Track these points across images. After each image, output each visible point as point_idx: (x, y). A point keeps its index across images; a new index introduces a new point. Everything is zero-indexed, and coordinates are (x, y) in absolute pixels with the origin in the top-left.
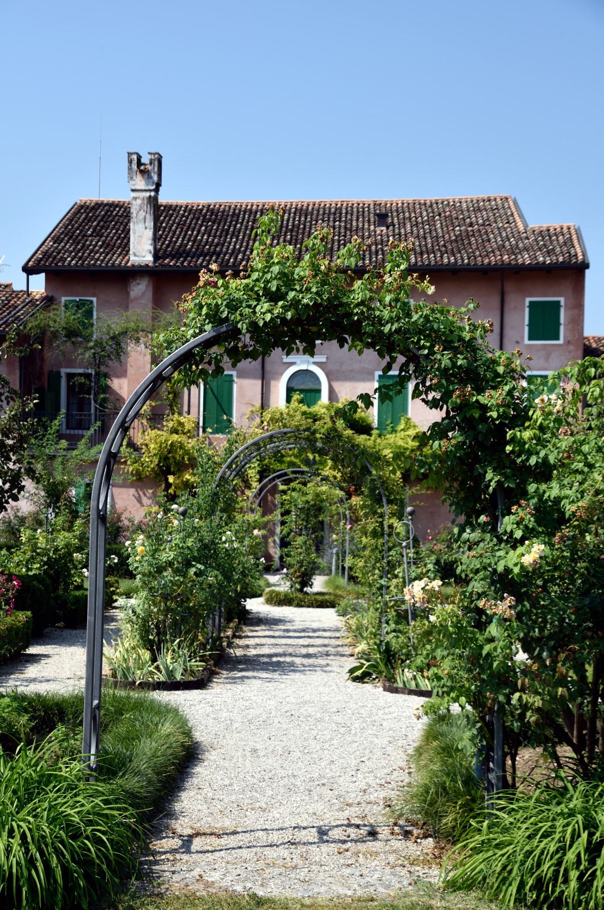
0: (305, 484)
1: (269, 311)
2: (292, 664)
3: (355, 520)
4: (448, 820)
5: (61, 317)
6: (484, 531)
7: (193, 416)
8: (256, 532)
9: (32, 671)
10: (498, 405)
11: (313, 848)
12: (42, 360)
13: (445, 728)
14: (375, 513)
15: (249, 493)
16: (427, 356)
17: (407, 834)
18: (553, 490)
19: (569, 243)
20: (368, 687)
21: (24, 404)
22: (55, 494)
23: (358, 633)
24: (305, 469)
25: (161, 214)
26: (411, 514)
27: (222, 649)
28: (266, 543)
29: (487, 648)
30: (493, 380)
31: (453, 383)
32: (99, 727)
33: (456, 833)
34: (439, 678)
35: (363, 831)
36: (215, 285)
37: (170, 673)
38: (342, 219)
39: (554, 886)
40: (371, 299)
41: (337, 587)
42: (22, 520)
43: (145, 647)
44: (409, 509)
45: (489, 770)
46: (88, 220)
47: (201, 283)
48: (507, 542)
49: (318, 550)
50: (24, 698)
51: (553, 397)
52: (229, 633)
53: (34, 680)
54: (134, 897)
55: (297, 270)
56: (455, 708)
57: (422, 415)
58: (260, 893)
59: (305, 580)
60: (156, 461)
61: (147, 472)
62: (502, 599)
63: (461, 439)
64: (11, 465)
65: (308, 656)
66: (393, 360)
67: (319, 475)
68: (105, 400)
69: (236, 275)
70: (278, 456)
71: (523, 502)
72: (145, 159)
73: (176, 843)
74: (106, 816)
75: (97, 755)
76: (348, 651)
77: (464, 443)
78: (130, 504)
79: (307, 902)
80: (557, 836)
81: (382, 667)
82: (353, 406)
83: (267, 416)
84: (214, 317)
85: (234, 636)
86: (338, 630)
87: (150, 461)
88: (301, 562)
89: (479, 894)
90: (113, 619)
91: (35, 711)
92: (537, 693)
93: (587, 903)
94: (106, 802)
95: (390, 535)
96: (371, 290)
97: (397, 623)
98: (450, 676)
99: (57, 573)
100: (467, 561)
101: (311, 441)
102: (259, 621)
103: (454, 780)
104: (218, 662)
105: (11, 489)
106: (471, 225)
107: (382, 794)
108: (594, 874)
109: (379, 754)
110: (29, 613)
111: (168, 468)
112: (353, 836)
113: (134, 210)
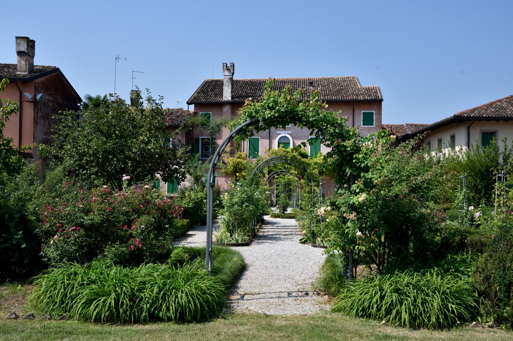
0: (284, 176)
1: (270, 114)
2: (280, 238)
3: (302, 188)
4: (333, 289)
5: (200, 119)
6: (346, 190)
7: (245, 152)
8: (267, 192)
9: (190, 240)
10: (350, 146)
11: (286, 299)
12: (193, 134)
13: (332, 258)
14: (309, 185)
15: (264, 179)
16: (325, 129)
17: (319, 294)
18: (369, 175)
19: (376, 92)
20: (306, 246)
21: (186, 149)
22: (197, 179)
23: (303, 227)
24: (284, 170)
25: (233, 83)
26: (321, 185)
27: (255, 233)
28: (271, 196)
29: (347, 230)
30: (348, 137)
31: (334, 138)
32: (212, 258)
33: (336, 293)
34: (330, 241)
35: (304, 293)
36: (251, 105)
37: (237, 241)
38: (295, 83)
39: (369, 310)
40: (305, 109)
41: (296, 212)
42: (186, 189)
43: (228, 232)
44: (321, 184)
45: (347, 272)
46: (209, 86)
47: (246, 104)
48: (354, 193)
49: (289, 199)
50: (186, 248)
51: (369, 143)
52: (258, 227)
53: (190, 243)
54: (224, 314)
55: (279, 100)
56: (336, 252)
57: (325, 150)
58: (268, 313)
59: (285, 209)
60: (232, 168)
61: (229, 172)
62: (352, 213)
63: (337, 158)
64: (182, 170)
65: (285, 235)
66: (313, 130)
67: (289, 172)
68: (214, 147)
69: (258, 102)
70: (275, 166)
71: (359, 180)
72: (229, 65)
73: (239, 297)
74: (214, 287)
75: (211, 267)
76: (300, 233)
77: (339, 159)
78: (222, 183)
79: (284, 316)
80: (370, 294)
81: (311, 238)
82: (300, 146)
83: (271, 152)
84: (250, 116)
85: (260, 228)
86: (296, 226)
87: (230, 168)
88: (283, 203)
89: (343, 313)
90: (218, 223)
91: (190, 253)
92: (364, 245)
93: (379, 315)
94: (214, 283)
95: (314, 193)
96: (305, 106)
97: (316, 223)
98: (334, 240)
99: (198, 207)
100: (340, 201)
101: (286, 160)
102: (268, 223)
103: (335, 276)
104: (254, 237)
105: (182, 178)
106: (342, 86)
107: (311, 281)
108: (382, 305)
109: (309, 268)
110: (188, 220)
111: (237, 171)
112: (300, 295)
113: (225, 82)
